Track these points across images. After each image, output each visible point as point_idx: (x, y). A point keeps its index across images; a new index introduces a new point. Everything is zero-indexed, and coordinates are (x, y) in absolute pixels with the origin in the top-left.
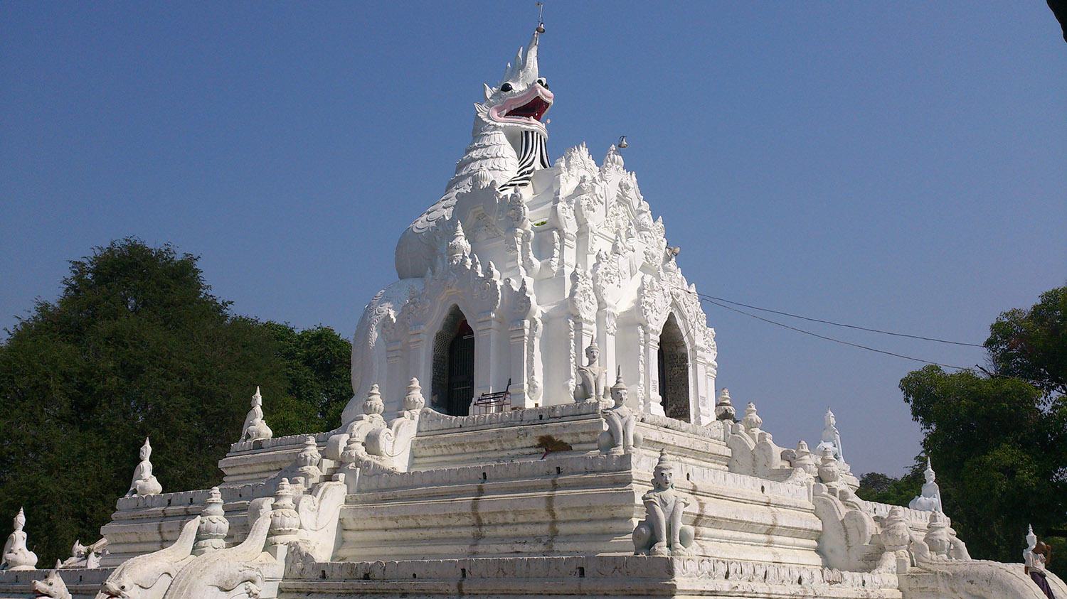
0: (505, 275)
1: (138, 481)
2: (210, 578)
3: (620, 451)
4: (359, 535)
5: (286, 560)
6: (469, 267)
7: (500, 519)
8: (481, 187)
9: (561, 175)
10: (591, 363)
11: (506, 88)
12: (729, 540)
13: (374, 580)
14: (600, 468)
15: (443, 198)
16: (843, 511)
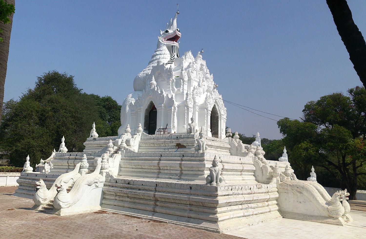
0: (167, 93)
1: (61, 148)
2: (85, 182)
3: (201, 151)
4: (125, 169)
5: (106, 177)
6: (156, 90)
7: (166, 168)
8: (160, 65)
9: (183, 61)
10: (192, 123)
11: (167, 32)
12: (230, 175)
13: (131, 185)
14: (195, 156)
15: (148, 66)
16: (262, 165)
